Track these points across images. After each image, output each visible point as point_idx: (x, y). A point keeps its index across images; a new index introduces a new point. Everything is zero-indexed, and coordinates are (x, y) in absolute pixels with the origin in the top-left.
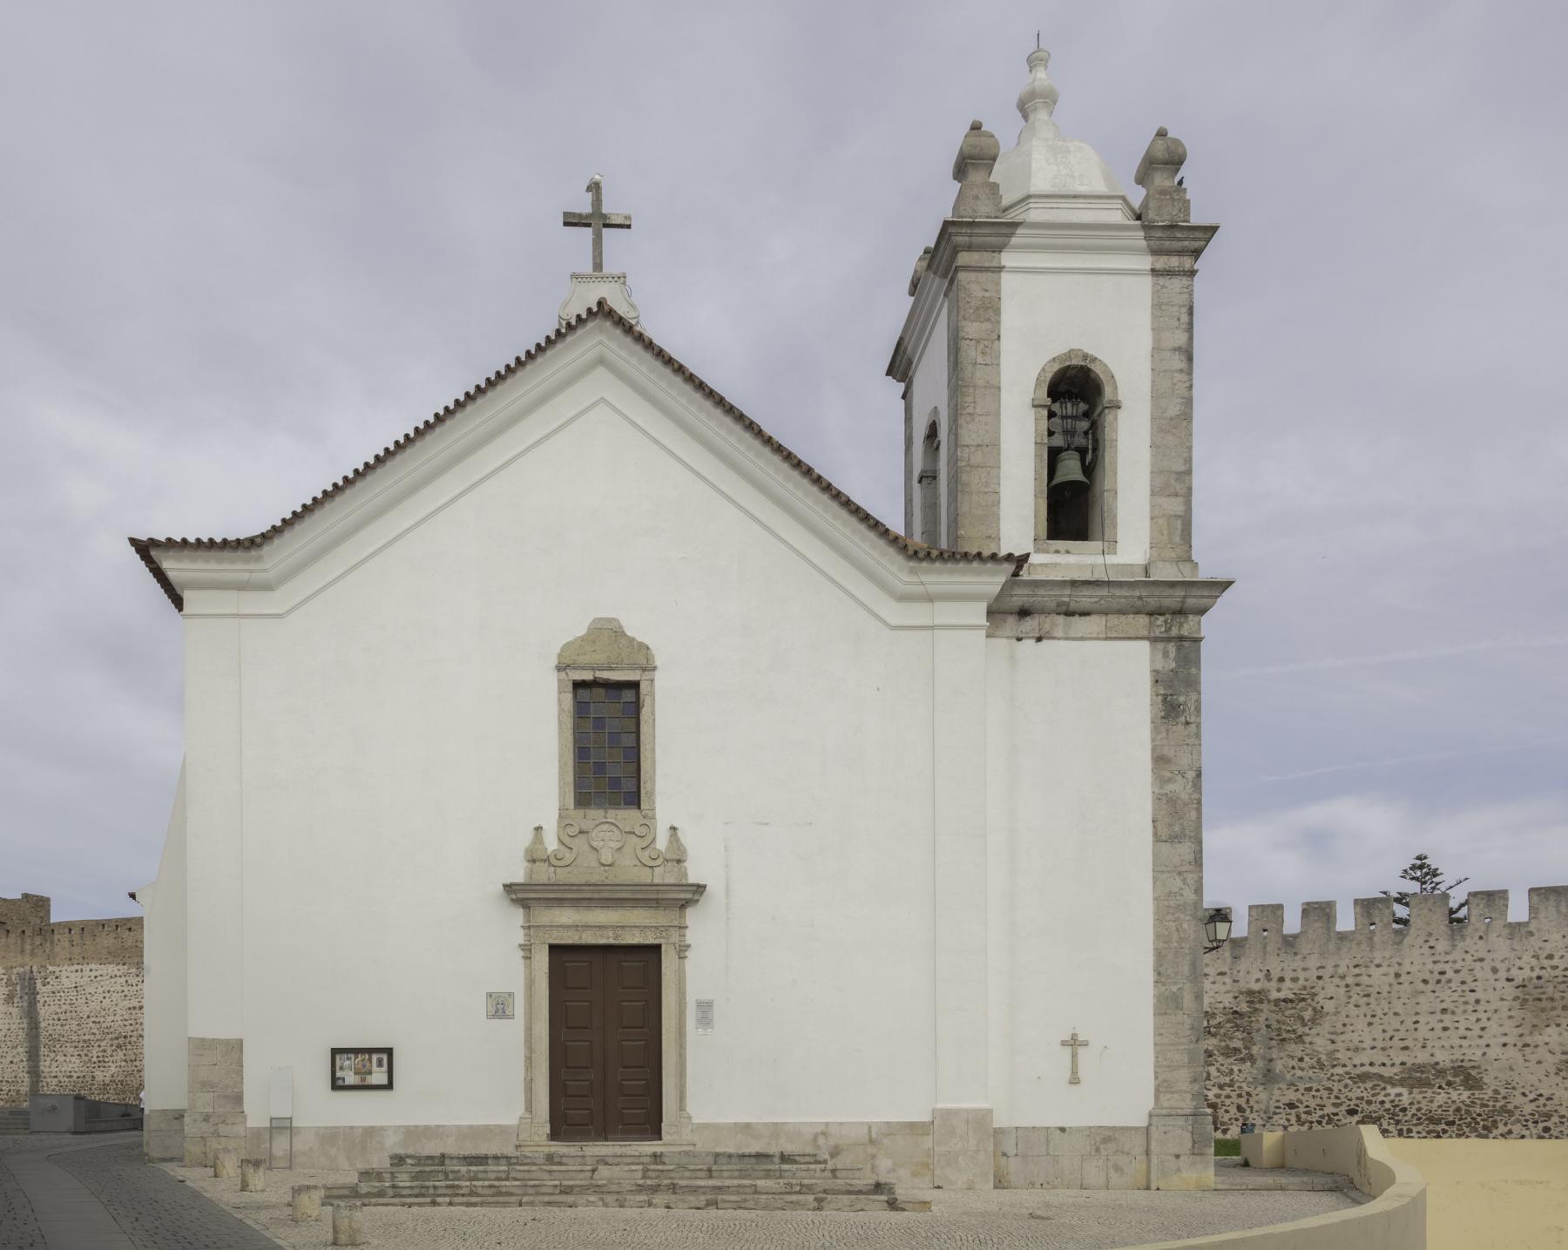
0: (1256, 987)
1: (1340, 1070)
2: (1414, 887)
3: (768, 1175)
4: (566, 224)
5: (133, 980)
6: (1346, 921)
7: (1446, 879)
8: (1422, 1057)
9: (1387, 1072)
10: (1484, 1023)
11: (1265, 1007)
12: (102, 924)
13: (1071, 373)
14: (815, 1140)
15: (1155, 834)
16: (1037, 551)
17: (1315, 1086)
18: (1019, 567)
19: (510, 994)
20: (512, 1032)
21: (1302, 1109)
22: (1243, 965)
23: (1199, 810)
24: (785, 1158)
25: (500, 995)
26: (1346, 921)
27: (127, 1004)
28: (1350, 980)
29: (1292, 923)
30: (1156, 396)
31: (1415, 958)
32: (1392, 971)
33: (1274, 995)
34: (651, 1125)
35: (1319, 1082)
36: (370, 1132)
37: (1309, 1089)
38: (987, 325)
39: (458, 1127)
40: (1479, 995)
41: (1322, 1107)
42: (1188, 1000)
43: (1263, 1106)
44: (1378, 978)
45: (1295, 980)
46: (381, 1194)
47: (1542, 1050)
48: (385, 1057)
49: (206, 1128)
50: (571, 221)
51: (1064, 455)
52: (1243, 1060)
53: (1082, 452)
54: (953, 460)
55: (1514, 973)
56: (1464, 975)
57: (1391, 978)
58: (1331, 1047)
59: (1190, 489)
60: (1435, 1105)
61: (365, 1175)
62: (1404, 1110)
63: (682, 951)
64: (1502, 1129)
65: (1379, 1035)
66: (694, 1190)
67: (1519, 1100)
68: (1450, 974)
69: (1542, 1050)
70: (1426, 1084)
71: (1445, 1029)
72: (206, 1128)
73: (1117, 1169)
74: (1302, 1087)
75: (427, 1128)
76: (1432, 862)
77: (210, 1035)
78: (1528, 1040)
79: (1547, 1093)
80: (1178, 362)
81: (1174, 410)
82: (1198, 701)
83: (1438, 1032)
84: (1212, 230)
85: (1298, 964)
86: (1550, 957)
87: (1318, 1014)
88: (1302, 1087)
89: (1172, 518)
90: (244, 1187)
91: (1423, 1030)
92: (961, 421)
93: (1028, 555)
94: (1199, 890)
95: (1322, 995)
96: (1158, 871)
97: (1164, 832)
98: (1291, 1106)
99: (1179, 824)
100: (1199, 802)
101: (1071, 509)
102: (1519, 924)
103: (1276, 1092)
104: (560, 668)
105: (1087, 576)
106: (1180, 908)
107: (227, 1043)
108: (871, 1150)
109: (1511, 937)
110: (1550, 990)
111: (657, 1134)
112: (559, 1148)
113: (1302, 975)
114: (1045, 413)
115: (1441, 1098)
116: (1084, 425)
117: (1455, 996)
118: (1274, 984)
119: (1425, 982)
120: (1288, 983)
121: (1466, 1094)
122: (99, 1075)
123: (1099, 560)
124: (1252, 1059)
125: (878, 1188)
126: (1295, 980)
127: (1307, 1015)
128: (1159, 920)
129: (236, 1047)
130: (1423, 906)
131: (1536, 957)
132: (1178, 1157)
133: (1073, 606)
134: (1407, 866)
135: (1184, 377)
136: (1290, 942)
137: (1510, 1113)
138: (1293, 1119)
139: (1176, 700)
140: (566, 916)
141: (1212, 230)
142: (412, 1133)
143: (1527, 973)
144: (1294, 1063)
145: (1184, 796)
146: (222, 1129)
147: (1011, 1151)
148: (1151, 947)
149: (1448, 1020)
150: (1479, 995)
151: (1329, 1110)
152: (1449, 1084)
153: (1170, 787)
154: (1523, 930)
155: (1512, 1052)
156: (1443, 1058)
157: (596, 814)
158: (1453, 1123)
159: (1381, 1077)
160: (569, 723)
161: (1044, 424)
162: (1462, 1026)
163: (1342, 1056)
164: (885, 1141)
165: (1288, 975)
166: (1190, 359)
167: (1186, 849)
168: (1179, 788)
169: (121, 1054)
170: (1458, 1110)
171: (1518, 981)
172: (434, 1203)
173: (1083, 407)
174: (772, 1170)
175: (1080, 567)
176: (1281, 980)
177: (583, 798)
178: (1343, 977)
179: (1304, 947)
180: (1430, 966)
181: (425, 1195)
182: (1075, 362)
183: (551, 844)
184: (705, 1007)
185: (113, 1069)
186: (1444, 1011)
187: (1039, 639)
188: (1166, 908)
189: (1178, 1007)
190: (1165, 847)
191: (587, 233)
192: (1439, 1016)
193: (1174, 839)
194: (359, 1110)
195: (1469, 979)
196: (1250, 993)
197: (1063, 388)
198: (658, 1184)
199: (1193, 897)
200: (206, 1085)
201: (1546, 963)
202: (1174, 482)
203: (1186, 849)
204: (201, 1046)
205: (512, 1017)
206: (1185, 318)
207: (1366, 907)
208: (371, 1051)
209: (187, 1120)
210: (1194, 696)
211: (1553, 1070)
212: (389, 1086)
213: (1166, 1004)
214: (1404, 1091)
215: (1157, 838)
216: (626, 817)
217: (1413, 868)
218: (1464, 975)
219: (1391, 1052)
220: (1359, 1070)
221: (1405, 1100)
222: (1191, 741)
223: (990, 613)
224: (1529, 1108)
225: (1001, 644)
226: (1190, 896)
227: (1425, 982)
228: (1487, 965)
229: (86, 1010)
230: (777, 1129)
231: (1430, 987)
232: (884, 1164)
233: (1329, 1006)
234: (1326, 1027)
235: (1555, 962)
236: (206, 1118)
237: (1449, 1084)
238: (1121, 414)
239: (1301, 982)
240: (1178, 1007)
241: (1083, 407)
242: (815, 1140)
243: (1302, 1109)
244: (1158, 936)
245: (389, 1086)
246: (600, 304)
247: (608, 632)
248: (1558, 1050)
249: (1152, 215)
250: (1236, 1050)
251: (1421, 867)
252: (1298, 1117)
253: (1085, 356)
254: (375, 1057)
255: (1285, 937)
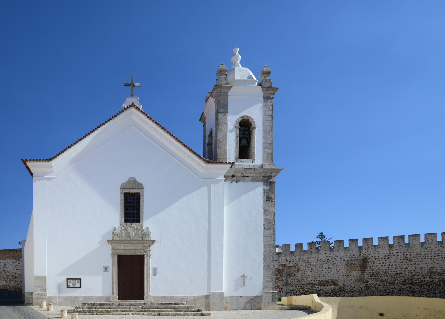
0: (284, 263)
1: (304, 282)
2: (320, 240)
3: (171, 308)
4: (125, 86)
5: (17, 263)
6: (305, 248)
7: (327, 239)
8: (323, 278)
9: (315, 282)
10: (338, 270)
11: (286, 268)
12: (10, 250)
13: (244, 120)
14: (181, 300)
15: (264, 228)
16: (236, 161)
17: (298, 286)
18: (232, 165)
19: (108, 266)
20: (109, 275)
21: (295, 291)
22: (280, 259)
23: (275, 222)
24: (175, 304)
25: (106, 266)
26: (305, 248)
27: (16, 269)
28: (306, 261)
29: (293, 249)
30: (264, 126)
31: (322, 256)
32: (316, 259)
33: (288, 265)
34: (141, 297)
35: (299, 285)
36: (76, 298)
37: (296, 287)
38: (225, 109)
39: (96, 297)
40: (337, 264)
41: (299, 291)
42: (272, 266)
43: (285, 291)
44: (313, 261)
45: (293, 262)
46: (80, 312)
47: (352, 276)
48: (79, 280)
49: (39, 296)
50: (126, 85)
51: (243, 139)
52: (281, 280)
53: (247, 139)
54: (216, 140)
55: (345, 259)
56: (333, 260)
57: (316, 261)
58: (301, 277)
59: (273, 147)
60: (326, 290)
61: (76, 308)
62: (319, 291)
63: (149, 256)
64: (342, 295)
65: (313, 274)
66: (154, 311)
67: (347, 288)
68: (330, 259)
69: (352, 276)
70: (325, 285)
71: (329, 272)
72: (39, 296)
73: (254, 305)
74: (295, 286)
75: (89, 297)
76: (324, 234)
77: (39, 275)
78: (349, 274)
79: (353, 286)
80: (270, 118)
81: (269, 128)
82: (275, 197)
83: (327, 273)
84: (277, 89)
85: (294, 258)
86: (354, 255)
87: (298, 270)
88: (295, 286)
89: (268, 154)
90: (48, 310)
91: (324, 273)
92: (218, 131)
93: (234, 163)
94: (274, 240)
95: (300, 265)
96: (265, 236)
97: (266, 227)
98: (292, 291)
99: (270, 225)
100: (275, 220)
101: (244, 151)
102: (347, 248)
103: (288, 288)
104: (122, 188)
105: (248, 167)
106: (270, 245)
107: (43, 277)
108: (195, 302)
109: (345, 250)
110: (354, 263)
111: (143, 299)
112: (120, 302)
113: (295, 260)
114: (238, 129)
115: (328, 288)
116: (247, 132)
117: (331, 265)
118: (288, 263)
119: (324, 261)
120: (291, 262)
121: (334, 287)
122: (9, 284)
123: (251, 164)
124: (282, 280)
125: (198, 311)
126: (293, 262)
127: (296, 270)
128: (265, 247)
129: (45, 278)
130: (320, 245)
131: (351, 255)
132: (269, 302)
133: (245, 175)
134: (318, 235)
135: (271, 122)
136: (292, 253)
137: (345, 291)
138: (292, 293)
139: (269, 197)
140: (122, 247)
141: (277, 89)
142: (85, 298)
143: (348, 259)
144: (293, 281)
145: (271, 219)
146: (42, 297)
147: (229, 302)
148: (262, 254)
149: (329, 270)
150: (337, 264)
151: (301, 291)
152: (330, 285)
153: (268, 216)
154: (348, 249)
155: (345, 277)
156: (328, 279)
157: (129, 224)
158: (331, 294)
159: (313, 284)
160: (123, 202)
161: (238, 132)
162: (333, 271)
163: (304, 279)
164: (198, 300)
165: (292, 261)
166: (273, 117)
167: (271, 231)
168: (270, 217)
169: (15, 280)
170: (332, 291)
171: (346, 261)
172: (92, 314)
173: (247, 128)
174: (171, 305)
175: (247, 165)
176: (290, 262)
177: (126, 221)
178: (305, 261)
179: (295, 254)
180: (325, 258)
181: (91, 312)
182: (245, 118)
183: (118, 231)
184: (155, 270)
185: (13, 284)
186: (329, 268)
187: (237, 182)
188: (267, 245)
189: (269, 267)
190: (266, 231)
191: (129, 88)
192: (327, 269)
193: (268, 229)
194: (75, 293)
195: (335, 261)
196: (283, 265)
197: (242, 124)
198: (145, 310)
199: (273, 242)
200: (38, 287)
201: (353, 257)
202: (269, 146)
203: (271, 231)
204: (38, 277)
205: (108, 271)
206: (271, 108)
207: (311, 244)
208: (76, 279)
209: (34, 295)
210: (274, 195)
211: (354, 281)
212: (80, 287)
213: (266, 267)
214: (319, 287)
215: (264, 228)
216: (135, 225)
217: (319, 235)
218: (333, 260)
219: (316, 278)
220: (308, 282)
221: (319, 289)
222: (273, 206)
223: (225, 176)
224: (349, 290)
225: (227, 183)
226: (272, 242)
227: (324, 261)
228: (339, 257)
229: (7, 270)
230: (172, 297)
231: (325, 263)
232: (198, 305)
233: (301, 268)
234: (300, 272)
235: (355, 256)
236: (38, 294)
237: (330, 285)
238: (256, 130)
239: (295, 262)
240: (269, 267)
241: (247, 128)
242: (181, 300)
243: (295, 291)
244: (265, 251)
245: (80, 287)
246: (132, 104)
247: (133, 182)
248: (356, 276)
249: (263, 85)
250: (279, 278)
251: (321, 235)
252: (294, 293)
253: (248, 117)
254: (77, 280)
255: (291, 252)
